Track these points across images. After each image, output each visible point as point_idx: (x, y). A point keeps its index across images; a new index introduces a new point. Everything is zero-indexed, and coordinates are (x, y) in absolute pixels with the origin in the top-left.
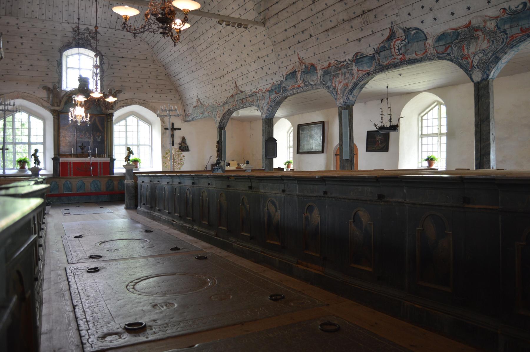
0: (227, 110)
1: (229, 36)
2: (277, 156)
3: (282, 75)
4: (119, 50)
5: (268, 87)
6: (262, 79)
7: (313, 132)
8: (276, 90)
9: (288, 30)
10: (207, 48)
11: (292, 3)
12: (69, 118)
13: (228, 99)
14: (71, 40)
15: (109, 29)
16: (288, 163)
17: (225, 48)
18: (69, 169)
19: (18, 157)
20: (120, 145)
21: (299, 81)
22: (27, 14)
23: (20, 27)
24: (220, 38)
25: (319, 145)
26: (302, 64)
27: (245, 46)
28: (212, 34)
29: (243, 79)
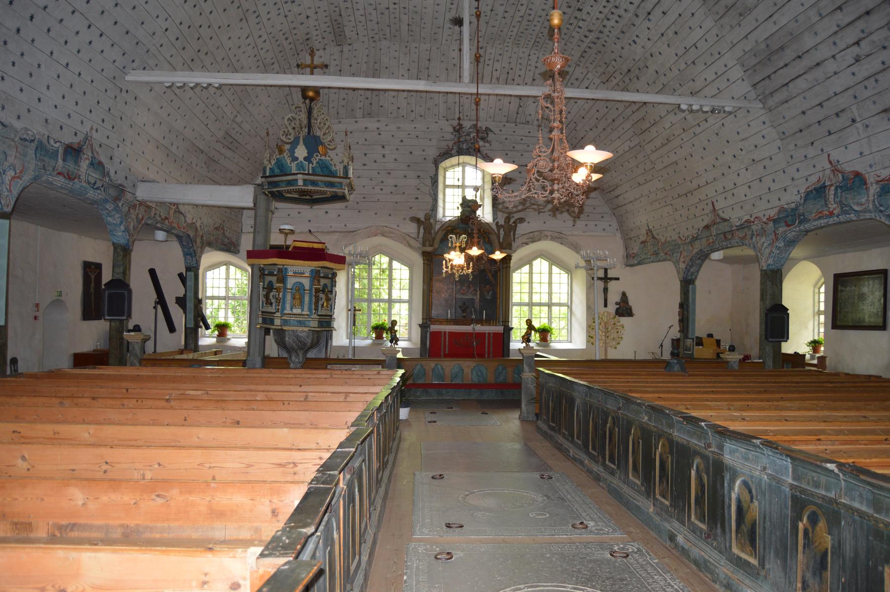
0: (698, 250)
1: (699, 126)
2: (788, 338)
3: (798, 191)
4: (522, 155)
5: (773, 213)
6: (761, 199)
7: (865, 290)
8: (787, 220)
9: (808, 113)
10: (663, 145)
11: (815, 64)
12: (443, 269)
13: (699, 233)
14: (451, 144)
15: (506, 124)
16: (815, 345)
17: (693, 145)
18: (443, 343)
19: (374, 321)
20: (520, 304)
21: (832, 205)
22: (391, 113)
23: (381, 133)
24: (684, 130)
25: (877, 315)
26: (836, 172)
27: (728, 142)
28: (671, 123)
29: (725, 198)
